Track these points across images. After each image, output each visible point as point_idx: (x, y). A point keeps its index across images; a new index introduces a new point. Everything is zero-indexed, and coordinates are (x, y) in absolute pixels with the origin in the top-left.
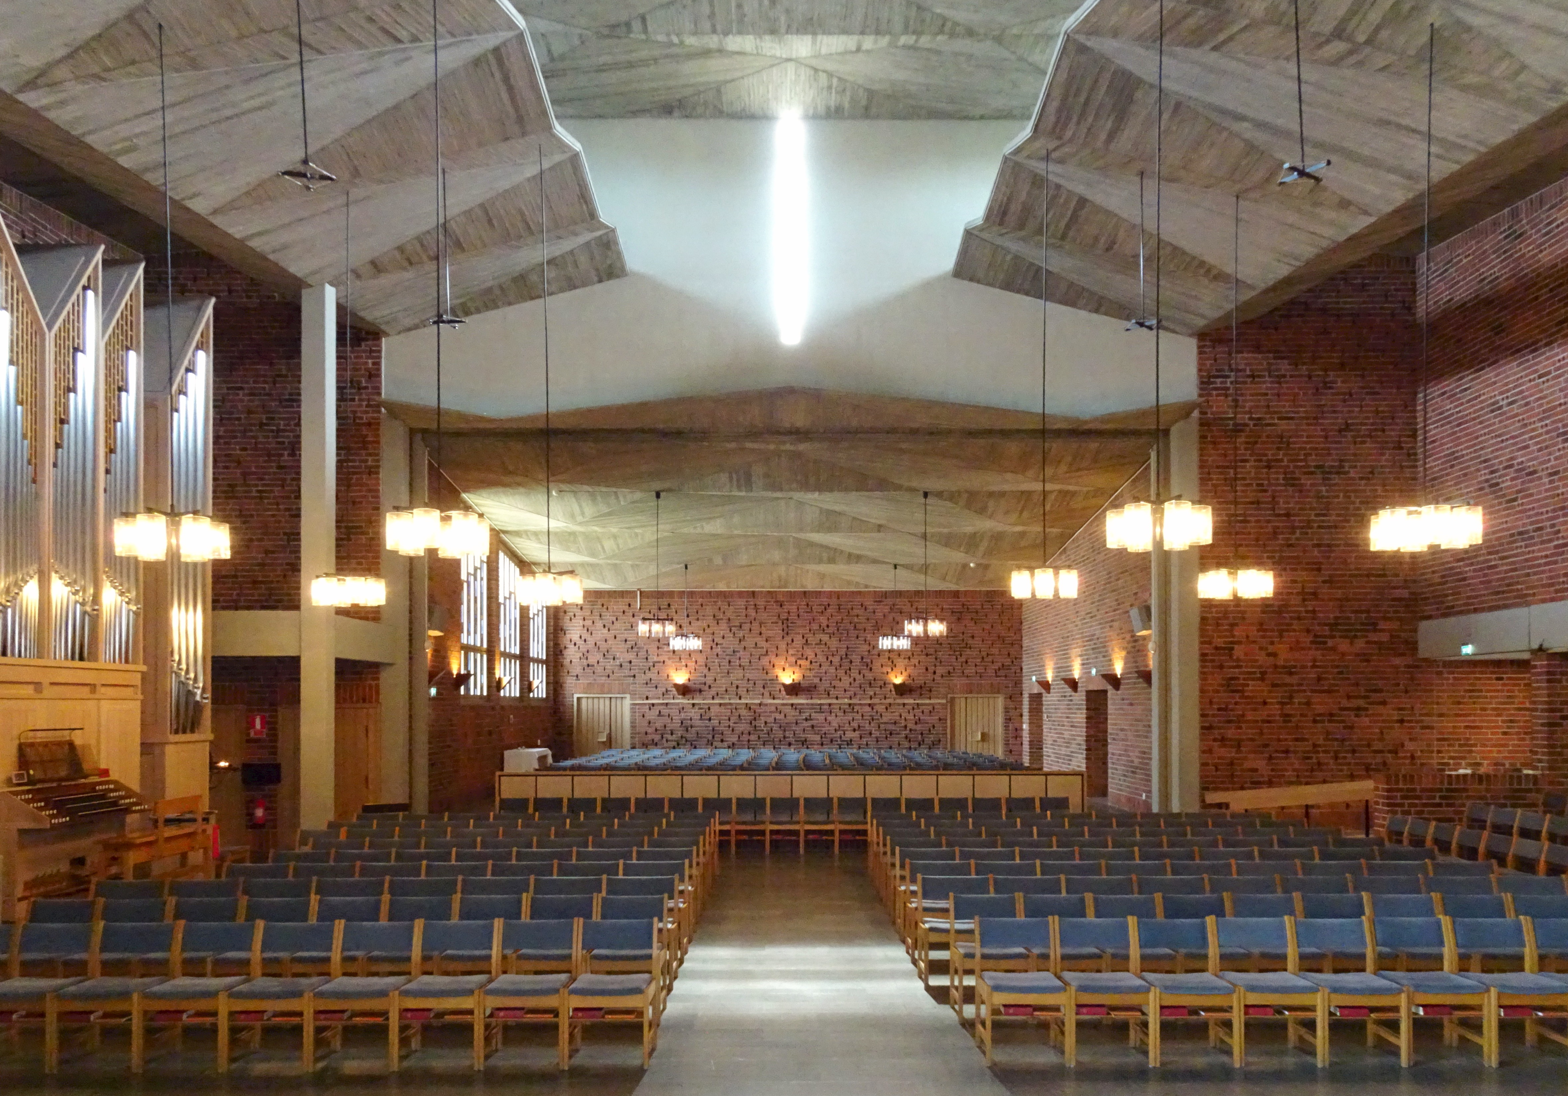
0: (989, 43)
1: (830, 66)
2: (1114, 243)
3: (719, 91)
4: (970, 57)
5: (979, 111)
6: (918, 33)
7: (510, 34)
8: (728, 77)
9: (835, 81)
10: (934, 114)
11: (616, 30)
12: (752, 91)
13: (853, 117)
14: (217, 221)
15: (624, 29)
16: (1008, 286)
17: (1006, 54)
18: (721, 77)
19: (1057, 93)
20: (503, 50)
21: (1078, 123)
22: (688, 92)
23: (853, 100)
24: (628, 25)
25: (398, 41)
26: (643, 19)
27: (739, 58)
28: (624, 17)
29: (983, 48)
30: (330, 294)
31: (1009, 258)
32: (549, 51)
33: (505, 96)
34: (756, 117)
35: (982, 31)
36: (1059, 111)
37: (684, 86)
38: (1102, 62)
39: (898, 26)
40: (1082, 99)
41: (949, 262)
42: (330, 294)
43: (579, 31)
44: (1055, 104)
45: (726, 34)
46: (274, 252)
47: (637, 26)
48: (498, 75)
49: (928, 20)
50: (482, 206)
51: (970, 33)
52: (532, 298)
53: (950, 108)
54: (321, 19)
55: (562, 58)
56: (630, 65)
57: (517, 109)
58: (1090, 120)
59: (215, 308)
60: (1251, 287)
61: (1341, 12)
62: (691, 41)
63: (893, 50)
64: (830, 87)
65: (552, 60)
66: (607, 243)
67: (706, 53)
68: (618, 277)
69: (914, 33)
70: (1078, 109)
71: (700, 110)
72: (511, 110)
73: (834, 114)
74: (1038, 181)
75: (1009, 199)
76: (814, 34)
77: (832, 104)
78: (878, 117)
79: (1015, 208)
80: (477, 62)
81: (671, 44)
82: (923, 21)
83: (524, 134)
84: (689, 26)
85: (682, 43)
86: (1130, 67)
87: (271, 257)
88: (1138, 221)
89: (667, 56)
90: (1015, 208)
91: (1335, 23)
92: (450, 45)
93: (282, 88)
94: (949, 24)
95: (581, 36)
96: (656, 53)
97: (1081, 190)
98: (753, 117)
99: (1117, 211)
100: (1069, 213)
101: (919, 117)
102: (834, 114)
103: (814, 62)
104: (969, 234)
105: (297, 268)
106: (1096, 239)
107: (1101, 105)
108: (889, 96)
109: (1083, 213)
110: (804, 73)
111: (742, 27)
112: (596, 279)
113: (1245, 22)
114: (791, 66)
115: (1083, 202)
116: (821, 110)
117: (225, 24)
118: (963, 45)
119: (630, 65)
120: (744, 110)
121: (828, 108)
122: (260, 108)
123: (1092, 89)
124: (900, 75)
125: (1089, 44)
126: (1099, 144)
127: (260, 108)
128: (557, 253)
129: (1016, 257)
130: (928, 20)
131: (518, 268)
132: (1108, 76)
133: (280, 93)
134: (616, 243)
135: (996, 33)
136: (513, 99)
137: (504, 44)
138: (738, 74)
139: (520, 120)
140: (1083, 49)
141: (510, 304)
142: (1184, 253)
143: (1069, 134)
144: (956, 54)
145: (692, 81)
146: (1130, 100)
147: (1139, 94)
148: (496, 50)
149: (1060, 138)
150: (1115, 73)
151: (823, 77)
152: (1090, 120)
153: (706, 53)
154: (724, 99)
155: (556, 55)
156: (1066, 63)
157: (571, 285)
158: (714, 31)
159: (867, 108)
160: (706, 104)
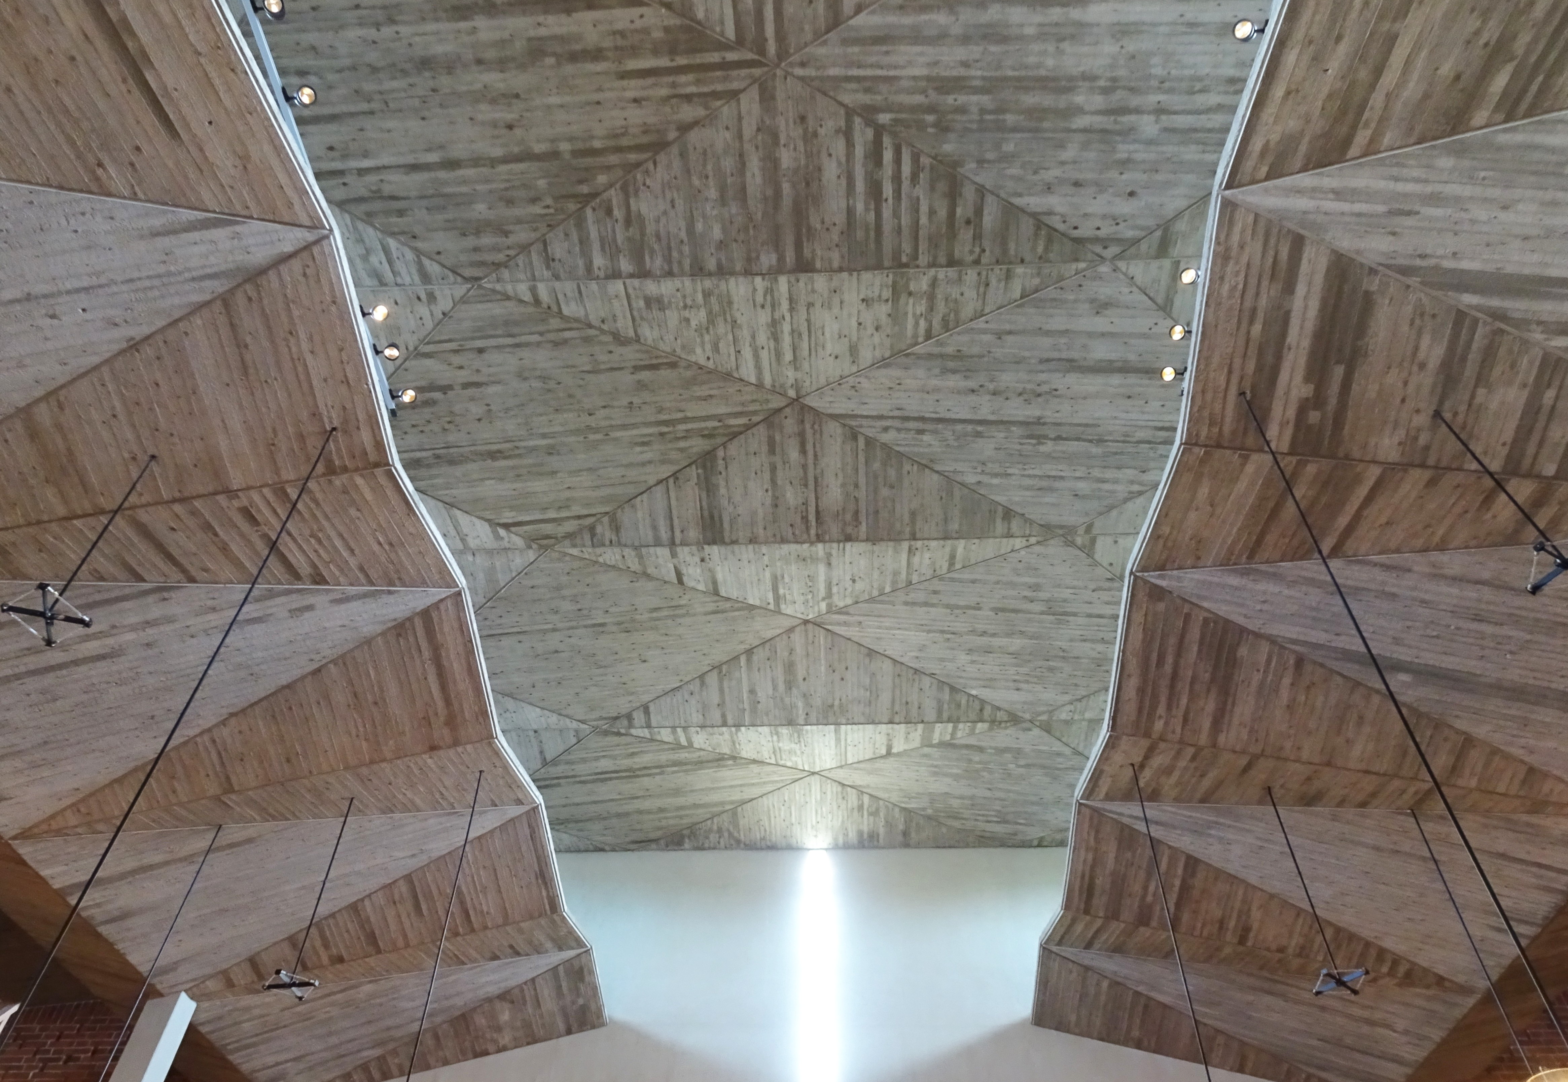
0: (1036, 731)
1: (859, 778)
2: (1247, 929)
3: (734, 813)
4: (1018, 752)
5: (1035, 833)
6: (954, 720)
7: (444, 592)
8: (746, 796)
9: (866, 799)
10: (985, 841)
11: (616, 725)
12: (774, 814)
13: (891, 846)
14: (25, 850)
15: (625, 722)
16: (1108, 1035)
17: (1057, 747)
18: (737, 796)
19: (1133, 665)
20: (434, 615)
21: (1169, 708)
22: (702, 813)
23: (889, 825)
24: (629, 717)
25: (297, 576)
26: (646, 709)
27: (755, 768)
28: (623, 705)
29: (1031, 739)
30: (184, 1010)
31: (1105, 984)
32: (541, 752)
33: (432, 679)
34: (776, 847)
35: (1027, 716)
36: (1141, 691)
37: (696, 806)
38: (1183, 608)
39: (931, 715)
40: (1168, 668)
41: (1023, 1004)
42: (184, 1010)
43: (575, 725)
44: (1133, 683)
45: (738, 726)
46: (107, 922)
47: (639, 717)
48: (427, 654)
49: (964, 702)
50: (408, 878)
51: (1014, 719)
52: (476, 1055)
53: (1000, 829)
54: (182, 500)
55: (555, 762)
56: (632, 774)
57: (448, 702)
58: (1184, 701)
59: (13, 1017)
60: (1465, 990)
61: (1508, 435)
62: (700, 739)
63: (926, 750)
64: (861, 807)
65: (545, 763)
66: (579, 973)
67: (719, 760)
68: (593, 1027)
69: (949, 721)
70: (1164, 683)
71: (713, 837)
72: (440, 704)
73: (867, 842)
74: (1127, 837)
75: (1093, 867)
76: (837, 724)
77: (865, 829)
78: (918, 846)
79: (1102, 881)
80: (401, 628)
81: (678, 747)
82: (959, 706)
83: (456, 743)
84: (696, 718)
85: (690, 744)
86: (1223, 610)
87: (103, 930)
88: (1334, 564)
89: (675, 764)
90: (1102, 881)
91: (1504, 451)
92: (365, 595)
93: (133, 628)
94: (988, 710)
95: (576, 731)
96: (664, 757)
97: (1186, 842)
98: (772, 847)
99: (1243, 874)
100: (1177, 883)
101: (967, 846)
102: (867, 842)
103: (840, 775)
104: (1046, 952)
105: (140, 958)
106: (1222, 924)
107: (1194, 680)
108: (929, 818)
109: (1198, 882)
110: (832, 789)
111: (754, 717)
112: (562, 1026)
113: (1374, 472)
114: (815, 781)
115: (1192, 863)
116: (853, 836)
117: (50, 493)
118: (1006, 737)
119: (632, 774)
120: (763, 839)
121: (860, 833)
122: (102, 657)
123: (1179, 655)
124: (939, 786)
125: (1163, 583)
126: (1203, 739)
127: (102, 657)
128: (512, 983)
129: (1115, 984)
130: (964, 702)
131: (459, 1002)
132: (1195, 633)
133: (130, 636)
134: (592, 972)
135: (1044, 717)
136: (443, 687)
137: (437, 605)
138: (756, 792)
139: (451, 722)
140: (1157, 593)
141: (446, 1062)
142: (1352, 937)
143: (1159, 725)
144: (1001, 751)
145: (706, 799)
146: (1233, 662)
147: (1243, 651)
148: (426, 614)
149: (1147, 734)
150: (1206, 621)
151: (852, 794)
152: (1184, 701)
153: (719, 760)
154: (742, 822)
155: (549, 758)
156: (1139, 618)
157: (530, 1037)
158: (725, 724)
159: (905, 834)
160: (720, 830)
